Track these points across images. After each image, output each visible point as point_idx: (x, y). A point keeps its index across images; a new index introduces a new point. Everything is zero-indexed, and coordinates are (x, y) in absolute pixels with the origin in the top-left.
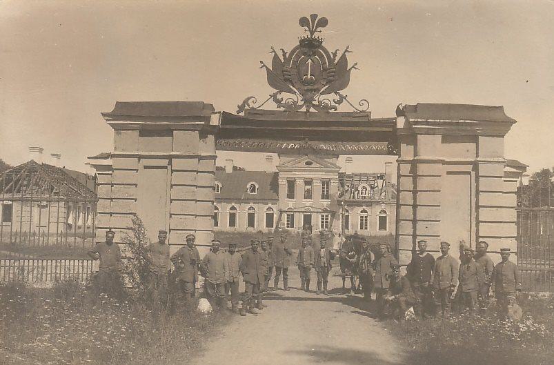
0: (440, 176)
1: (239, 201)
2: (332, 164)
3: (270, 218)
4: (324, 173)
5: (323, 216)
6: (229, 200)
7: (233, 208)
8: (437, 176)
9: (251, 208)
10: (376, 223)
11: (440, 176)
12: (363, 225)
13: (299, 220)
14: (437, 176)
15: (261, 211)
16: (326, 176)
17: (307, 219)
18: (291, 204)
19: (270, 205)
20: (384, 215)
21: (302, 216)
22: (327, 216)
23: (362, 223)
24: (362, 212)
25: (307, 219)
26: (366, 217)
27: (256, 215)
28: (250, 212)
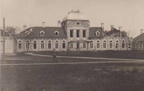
0: (4, 19)
1: (52, 38)
2: (86, 24)
3: (64, 45)
4: (84, 27)
5: (84, 44)
6: (49, 38)
7: (57, 41)
8: (4, 22)
9: (98, 41)
10: (61, 46)
11: (4, 19)
12: (57, 46)
13: (75, 45)
14: (4, 22)
15: (60, 42)
16: (85, 29)
17: (78, 45)
18: (72, 39)
19: (64, 40)
20: (20, 43)
21: (76, 43)
22: (85, 44)
23: (84, 46)
24: (97, 42)
25: (78, 45)
26: (105, 44)
27: (22, 44)
28: (123, 43)
